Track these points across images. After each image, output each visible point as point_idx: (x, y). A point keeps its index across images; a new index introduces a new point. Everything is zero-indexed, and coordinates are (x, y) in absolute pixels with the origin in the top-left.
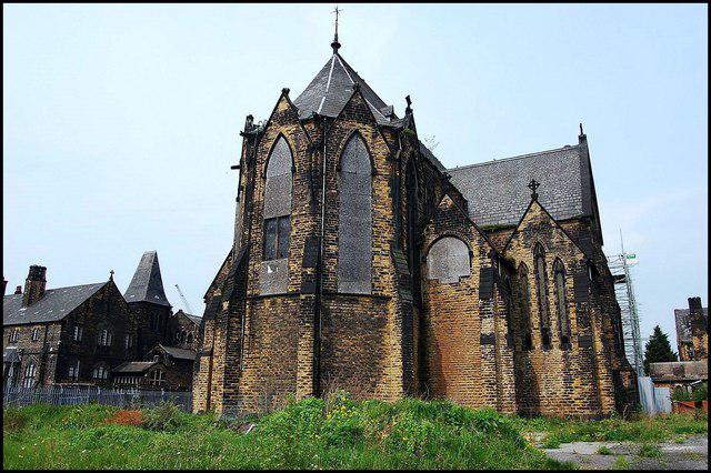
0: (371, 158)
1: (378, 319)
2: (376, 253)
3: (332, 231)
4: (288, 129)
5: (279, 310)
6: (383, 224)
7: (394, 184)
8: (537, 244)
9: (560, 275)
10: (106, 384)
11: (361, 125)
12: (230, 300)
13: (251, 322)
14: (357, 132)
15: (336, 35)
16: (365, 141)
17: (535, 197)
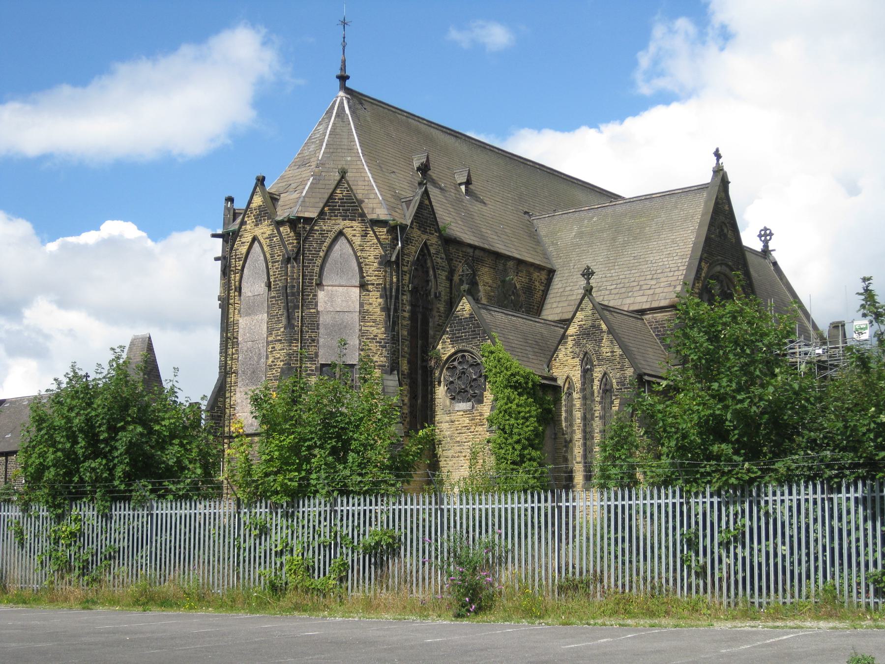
0: (359, 264)
7: (386, 294)
10: (476, 612)
11: (347, 223)
15: (344, 62)
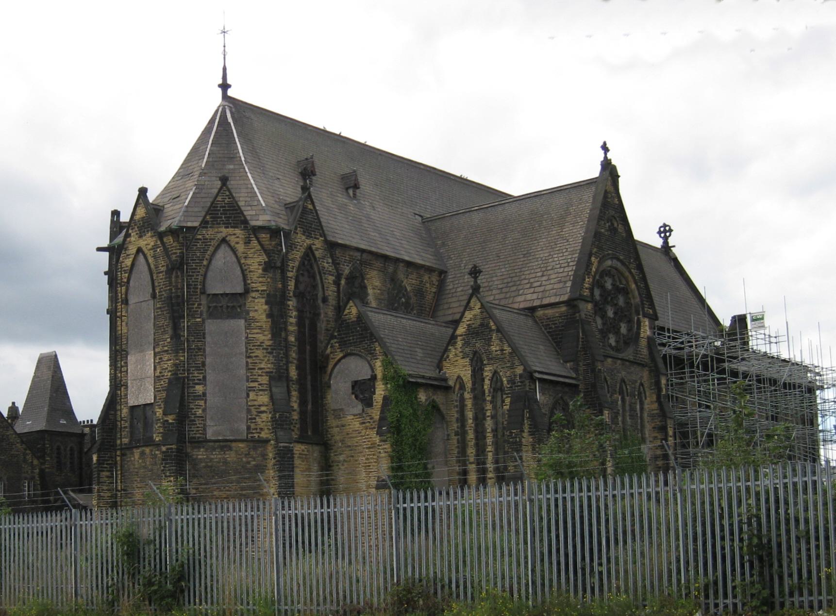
0: (243, 271)
1: (256, 466)
2: (251, 389)
3: (198, 369)
4: (148, 242)
5: (148, 461)
6: (259, 353)
8: (475, 353)
9: (499, 393)
11: (230, 230)
12: (99, 451)
13: (121, 470)
14: (224, 240)
15: (225, 69)
16: (234, 251)
17: (476, 289)
